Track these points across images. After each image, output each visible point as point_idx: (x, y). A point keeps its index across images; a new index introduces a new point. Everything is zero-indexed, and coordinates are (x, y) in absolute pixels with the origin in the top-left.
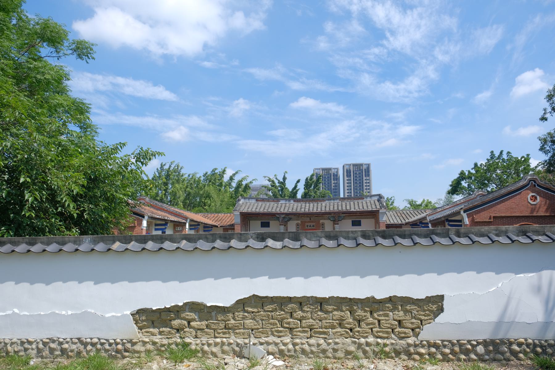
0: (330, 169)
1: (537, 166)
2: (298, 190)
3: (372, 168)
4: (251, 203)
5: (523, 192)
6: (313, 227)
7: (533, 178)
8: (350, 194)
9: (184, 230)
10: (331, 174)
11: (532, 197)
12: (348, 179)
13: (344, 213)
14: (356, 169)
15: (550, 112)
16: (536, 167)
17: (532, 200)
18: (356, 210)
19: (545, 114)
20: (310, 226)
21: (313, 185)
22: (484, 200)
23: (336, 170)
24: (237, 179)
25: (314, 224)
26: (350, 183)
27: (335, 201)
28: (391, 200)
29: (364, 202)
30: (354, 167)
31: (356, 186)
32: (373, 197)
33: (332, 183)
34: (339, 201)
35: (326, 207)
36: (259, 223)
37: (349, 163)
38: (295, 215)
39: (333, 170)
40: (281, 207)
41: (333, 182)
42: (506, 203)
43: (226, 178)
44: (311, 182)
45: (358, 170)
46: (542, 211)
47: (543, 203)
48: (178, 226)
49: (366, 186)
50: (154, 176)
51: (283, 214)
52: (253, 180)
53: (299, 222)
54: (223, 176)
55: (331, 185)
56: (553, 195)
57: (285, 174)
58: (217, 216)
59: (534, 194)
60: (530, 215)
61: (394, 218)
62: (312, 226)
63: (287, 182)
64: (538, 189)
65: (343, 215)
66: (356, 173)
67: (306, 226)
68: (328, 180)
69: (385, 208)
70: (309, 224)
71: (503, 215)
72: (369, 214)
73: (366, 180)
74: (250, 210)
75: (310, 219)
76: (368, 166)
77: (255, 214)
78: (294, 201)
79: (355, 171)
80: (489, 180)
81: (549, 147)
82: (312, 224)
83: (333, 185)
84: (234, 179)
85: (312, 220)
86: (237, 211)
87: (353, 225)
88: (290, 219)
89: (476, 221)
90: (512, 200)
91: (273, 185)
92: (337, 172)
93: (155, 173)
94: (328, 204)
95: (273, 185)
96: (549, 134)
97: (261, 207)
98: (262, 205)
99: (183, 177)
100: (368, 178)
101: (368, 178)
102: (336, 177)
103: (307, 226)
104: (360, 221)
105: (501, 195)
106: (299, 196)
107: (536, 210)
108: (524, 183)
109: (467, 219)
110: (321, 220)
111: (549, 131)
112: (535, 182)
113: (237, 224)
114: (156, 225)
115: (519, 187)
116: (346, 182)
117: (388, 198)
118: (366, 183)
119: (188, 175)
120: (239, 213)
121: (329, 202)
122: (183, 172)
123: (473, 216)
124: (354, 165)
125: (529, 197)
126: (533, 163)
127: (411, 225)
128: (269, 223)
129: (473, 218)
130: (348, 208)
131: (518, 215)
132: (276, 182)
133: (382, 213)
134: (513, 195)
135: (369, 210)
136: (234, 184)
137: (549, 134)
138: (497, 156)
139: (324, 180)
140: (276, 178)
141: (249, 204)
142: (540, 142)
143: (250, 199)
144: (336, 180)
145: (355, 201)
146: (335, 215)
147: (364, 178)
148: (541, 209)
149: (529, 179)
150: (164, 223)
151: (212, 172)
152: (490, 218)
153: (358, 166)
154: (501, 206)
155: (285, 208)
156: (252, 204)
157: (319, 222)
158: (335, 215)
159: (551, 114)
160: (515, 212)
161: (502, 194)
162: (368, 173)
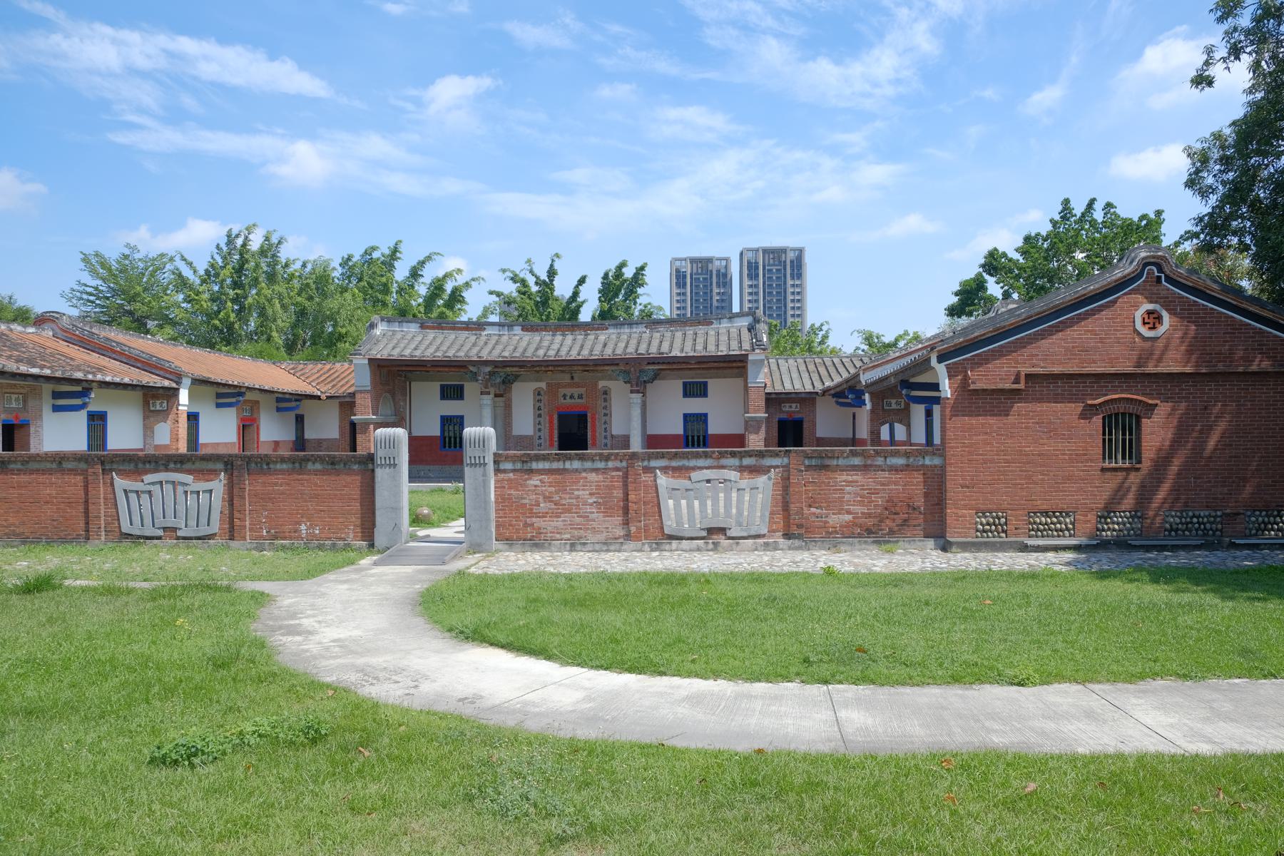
0: (710, 260)
1: (1179, 242)
2: (583, 302)
3: (808, 260)
4: (407, 332)
5: (1123, 298)
6: (579, 398)
7: (1154, 257)
8: (683, 312)
9: (174, 409)
10: (711, 271)
11: (1146, 316)
12: (750, 283)
13: (652, 361)
14: (771, 261)
15: (1224, 59)
16: (1177, 244)
17: (1147, 326)
18: (684, 355)
19: (1207, 63)
20: (572, 397)
21: (623, 292)
22: (1003, 324)
23: (724, 263)
24: (429, 274)
25: (582, 390)
26: (757, 294)
27: (635, 330)
28: (821, 330)
29: (712, 333)
30: (767, 256)
31: (769, 302)
32: (736, 319)
33: (714, 294)
34: (644, 329)
35: (605, 345)
36: (435, 387)
37: (755, 246)
38: (521, 367)
39: (717, 263)
40: (486, 343)
41: (716, 290)
42: (1068, 332)
43: (401, 272)
44: (618, 283)
45: (777, 263)
46: (1176, 360)
47: (1179, 334)
48: (156, 397)
49: (793, 301)
50: (212, 266)
51: (486, 363)
52: (473, 280)
53: (543, 385)
54: (392, 266)
55: (711, 298)
56: (1212, 309)
57: (553, 261)
58: (330, 370)
59: (1150, 307)
60: (1139, 371)
61: (795, 375)
62: (576, 396)
63: (282, 247)
64: (1168, 289)
65: (651, 367)
66: (769, 270)
67: (560, 395)
68: (705, 286)
69: (764, 350)
70: (568, 391)
71: (1057, 369)
72: (722, 365)
73: (793, 286)
74: (396, 354)
75: (572, 378)
76: (800, 252)
77: (441, 364)
78: (522, 330)
79: (769, 265)
80: (1052, 277)
81: (1215, 176)
82: (576, 391)
83: (716, 297)
84: (422, 276)
85: (576, 380)
86: (360, 354)
87: (686, 395)
88: (656, 376)
89: (972, 387)
90: (1089, 324)
91: (524, 291)
92: (726, 267)
93: (212, 258)
94: (614, 337)
95: (524, 291)
96: (1215, 139)
97: (431, 344)
98: (434, 338)
99: (290, 270)
100: (797, 282)
101: (797, 282)
102: (724, 279)
103: (565, 396)
104: (705, 384)
105: (1053, 308)
106: (585, 316)
107: (1155, 357)
108: (1126, 272)
109: (947, 381)
110: (603, 378)
111: (1216, 129)
112: (1160, 270)
113: (361, 392)
114: (56, 395)
115: (1109, 284)
116: (747, 290)
117: (813, 325)
118: (793, 293)
119: (301, 263)
120: (366, 362)
121: (619, 331)
122: (284, 254)
123: (966, 372)
124: (766, 251)
125: (1139, 315)
126: (1170, 234)
127: (834, 396)
128: (461, 388)
129: (966, 378)
130: (665, 348)
131: (1100, 370)
132: (531, 281)
133: (755, 362)
134: (1092, 309)
135: (719, 354)
136: (422, 289)
137: (1215, 139)
138: (1079, 215)
139: (696, 286)
140: (531, 272)
141: (399, 336)
142: (1189, 161)
143: (404, 324)
144: (724, 286)
145: (687, 328)
146: (628, 368)
147: (790, 282)
148: (1171, 354)
149: (1143, 259)
150: (79, 389)
151: (362, 256)
152: (1017, 381)
153: (775, 254)
154: (1053, 343)
155: (493, 348)
156: (411, 335)
157: (596, 385)
158: (628, 368)
159: (1225, 65)
160: (1094, 362)
161: (1058, 305)
162: (798, 270)
